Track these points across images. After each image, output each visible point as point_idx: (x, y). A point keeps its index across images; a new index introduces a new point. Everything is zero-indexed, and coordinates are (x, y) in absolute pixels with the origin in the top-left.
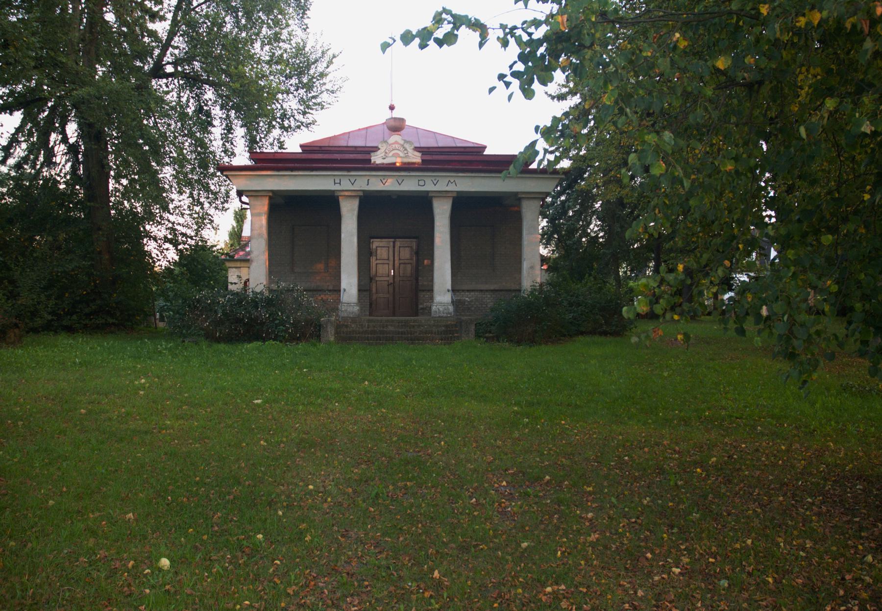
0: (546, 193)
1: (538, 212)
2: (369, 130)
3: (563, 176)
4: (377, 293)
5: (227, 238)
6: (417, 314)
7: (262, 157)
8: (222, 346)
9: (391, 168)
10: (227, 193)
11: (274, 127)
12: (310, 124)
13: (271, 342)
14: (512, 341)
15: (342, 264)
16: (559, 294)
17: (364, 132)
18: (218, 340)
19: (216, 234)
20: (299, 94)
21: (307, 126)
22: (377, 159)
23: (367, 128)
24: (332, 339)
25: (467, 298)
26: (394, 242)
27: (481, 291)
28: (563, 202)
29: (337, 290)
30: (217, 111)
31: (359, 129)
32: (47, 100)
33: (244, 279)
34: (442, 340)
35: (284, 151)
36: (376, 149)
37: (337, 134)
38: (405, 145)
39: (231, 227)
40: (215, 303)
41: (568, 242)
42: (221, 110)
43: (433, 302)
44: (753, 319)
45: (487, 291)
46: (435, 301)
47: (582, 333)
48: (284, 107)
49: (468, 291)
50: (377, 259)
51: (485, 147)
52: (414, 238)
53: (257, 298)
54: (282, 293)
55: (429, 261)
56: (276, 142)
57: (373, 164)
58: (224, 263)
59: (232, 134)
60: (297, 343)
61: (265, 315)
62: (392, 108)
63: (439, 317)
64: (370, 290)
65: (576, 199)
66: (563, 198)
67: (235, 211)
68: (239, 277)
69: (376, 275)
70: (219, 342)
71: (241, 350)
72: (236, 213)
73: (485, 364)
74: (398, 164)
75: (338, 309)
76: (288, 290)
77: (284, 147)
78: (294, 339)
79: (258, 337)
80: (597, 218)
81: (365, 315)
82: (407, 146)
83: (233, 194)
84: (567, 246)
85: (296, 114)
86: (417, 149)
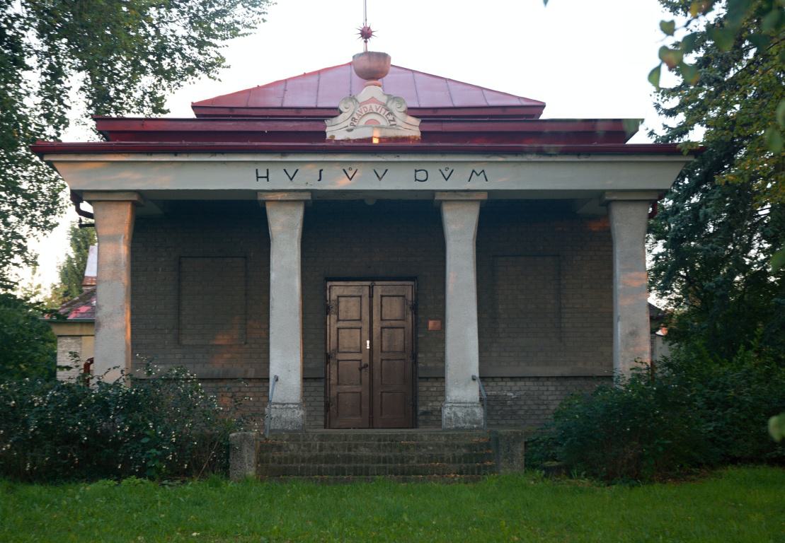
0: (662, 190)
1: (643, 227)
2: (323, 77)
3: (691, 159)
4: (338, 384)
5: (57, 280)
6: (415, 426)
7: (120, 127)
8: (35, 490)
9: (362, 148)
10: (55, 196)
11: (143, 71)
12: (212, 64)
13: (134, 479)
14: (595, 475)
15: (271, 330)
16: (687, 386)
17: (314, 80)
18: (29, 478)
19: (34, 272)
20: (191, 8)
21: (207, 68)
22: (337, 131)
23: (319, 72)
24: (251, 472)
25: (510, 391)
26: (371, 288)
27: (538, 378)
28: (695, 207)
30: (31, 38)
31: (305, 74)
32: (121, 235)
33: (84, 359)
34: (461, 473)
35: (163, 116)
36: (334, 112)
37: (261, 84)
38: (389, 105)
39: (66, 258)
40: (25, 405)
41: (706, 284)
42: (39, 37)
43: (444, 400)
44: (58, 377)
45: (548, 378)
46: (448, 399)
47: (734, 461)
48: (162, 31)
49: (512, 378)
50: (338, 320)
51: (541, 106)
52: (407, 279)
53: (108, 395)
54: (155, 385)
55: (438, 323)
56: (147, 98)
57: (329, 141)
58: (49, 329)
59: (61, 82)
60: (183, 482)
61: (121, 426)
62: (366, 34)
63: (457, 429)
64: (325, 379)
65: (721, 201)
66: (695, 200)
67: (73, 228)
68: (75, 355)
69: (337, 350)
70: (31, 482)
71: (73, 496)
72: (74, 233)
73: (542, 522)
74: (376, 141)
75: (263, 415)
76: (168, 380)
77: (165, 108)
78: (178, 472)
79: (107, 470)
80: (764, 237)
81: (316, 427)
82: (393, 106)
83: (65, 196)
84: (705, 291)
85: (185, 47)
86: (412, 111)
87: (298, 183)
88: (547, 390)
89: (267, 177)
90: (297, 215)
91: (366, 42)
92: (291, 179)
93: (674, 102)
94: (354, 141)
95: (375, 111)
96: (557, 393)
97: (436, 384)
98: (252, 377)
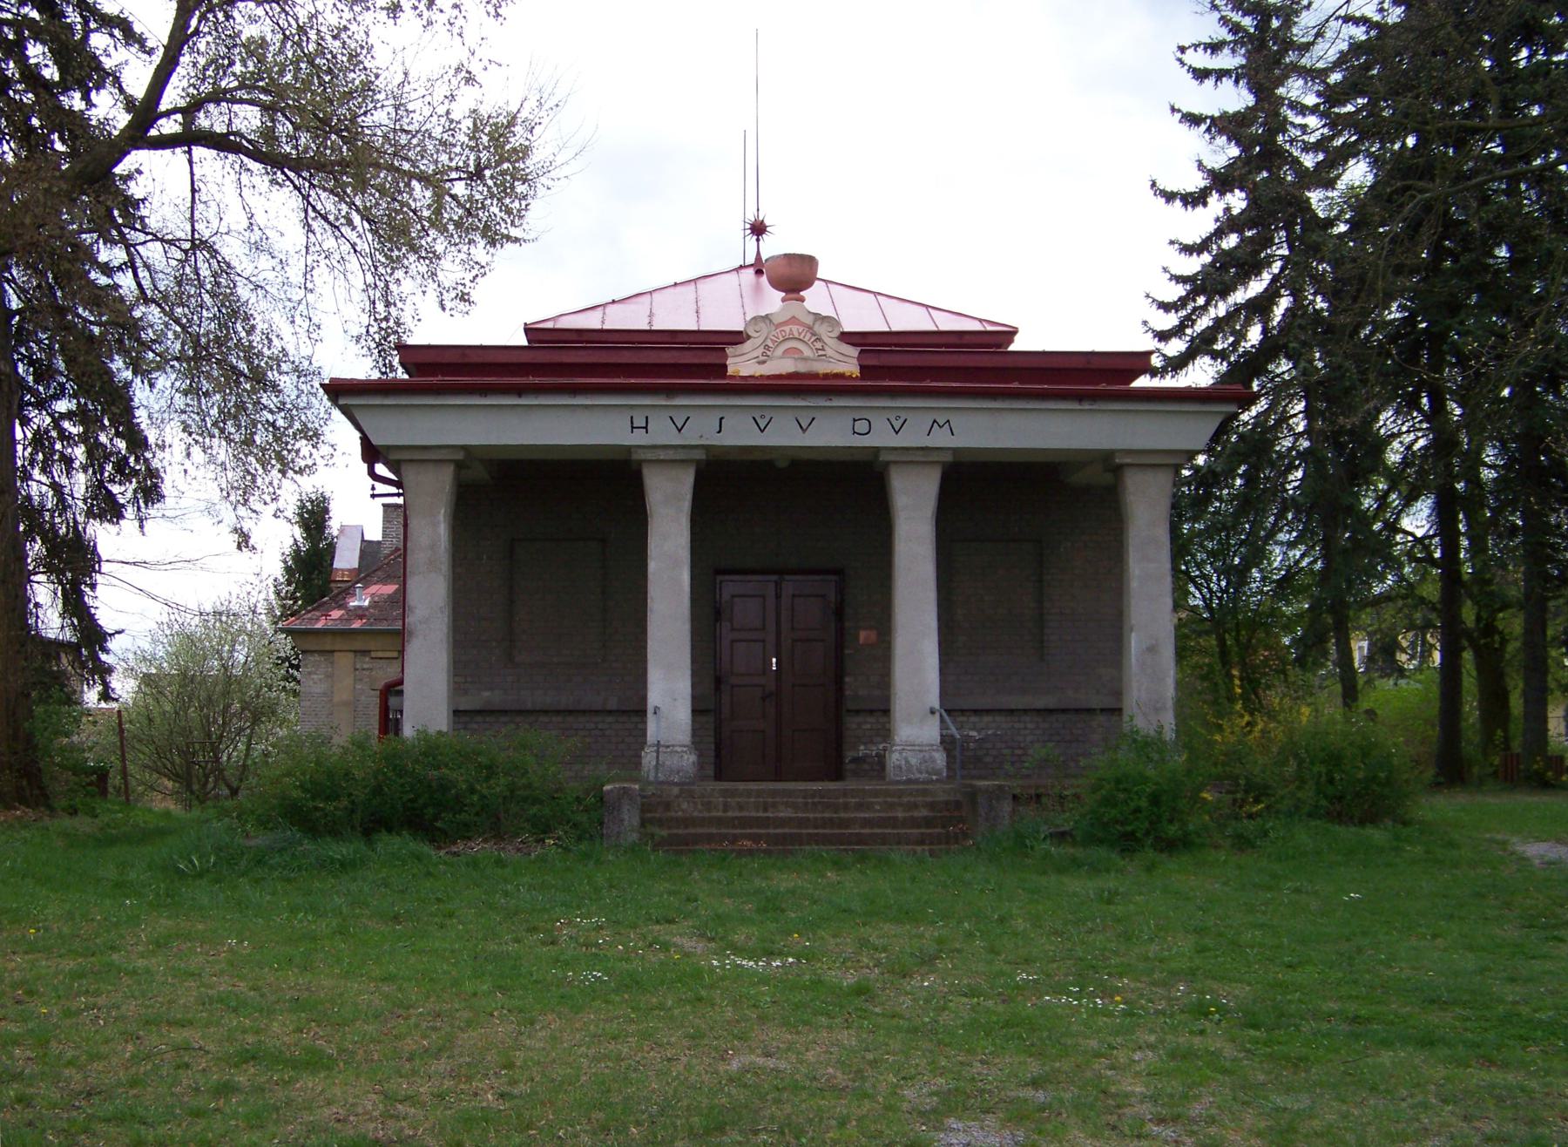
6: (838, 776)
22: (742, 364)
27: (1011, 712)
29: (638, 711)
38: (817, 328)
39: (291, 541)
45: (1025, 711)
49: (976, 712)
51: (1011, 334)
52: (828, 572)
57: (732, 377)
62: (758, 229)
63: (909, 781)
87: (690, 437)
88: (1026, 728)
89: (646, 428)
90: (687, 479)
91: (758, 240)
92: (680, 430)
93: (1170, 321)
94: (769, 377)
95: (796, 335)
96: (1038, 732)
97: (870, 719)
98: (615, 708)
